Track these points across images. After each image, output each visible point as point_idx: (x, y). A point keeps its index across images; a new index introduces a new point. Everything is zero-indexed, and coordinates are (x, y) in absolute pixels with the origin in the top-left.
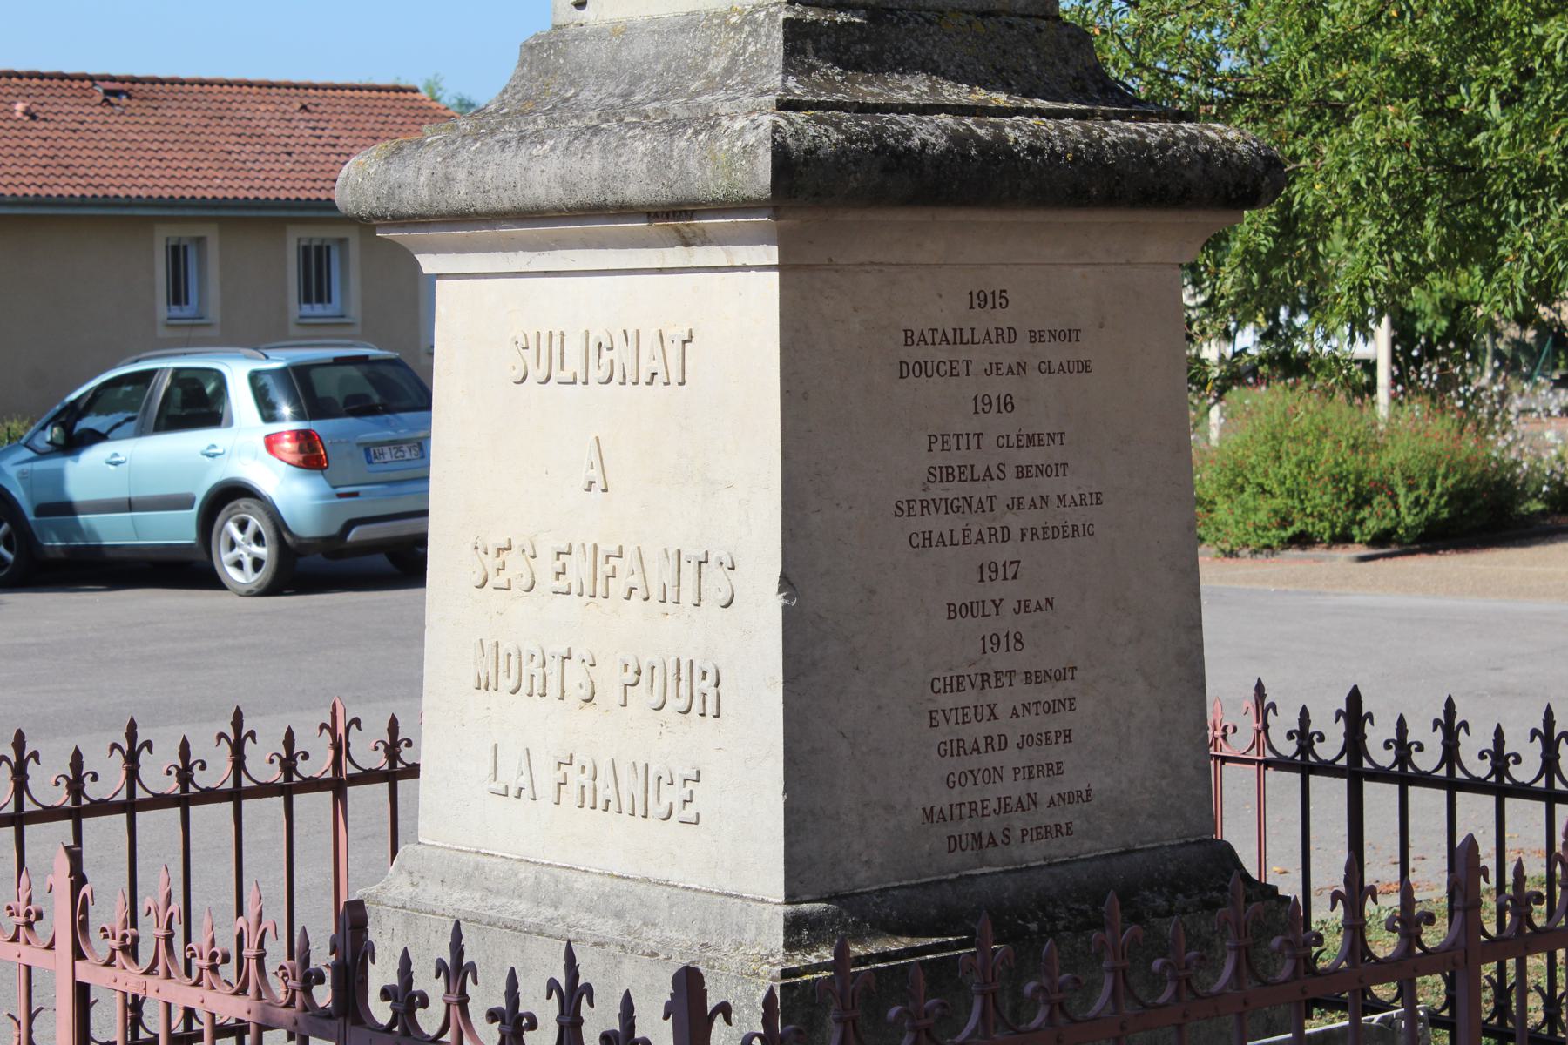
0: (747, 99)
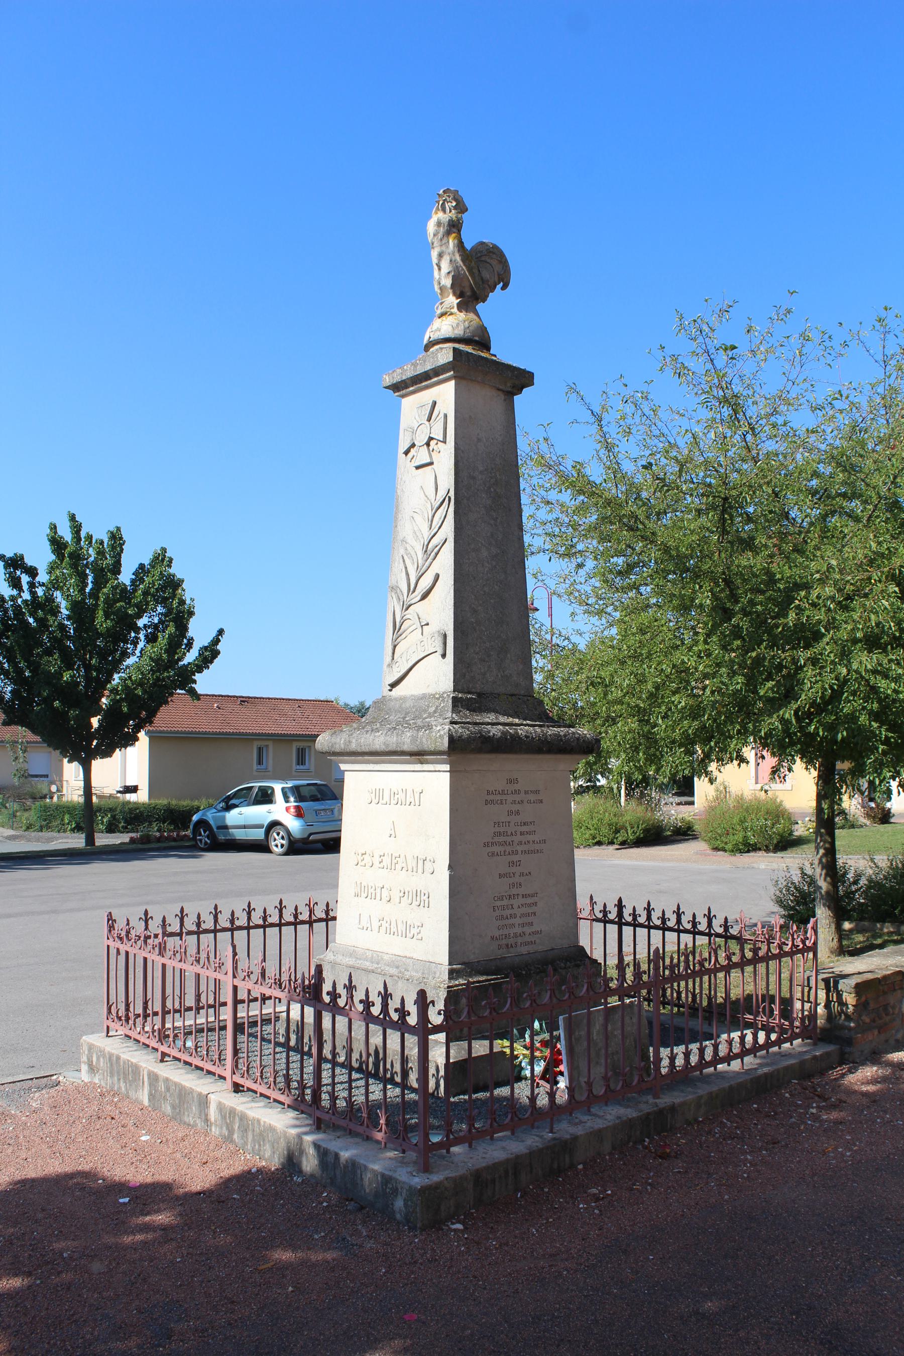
0: (441, 720)
